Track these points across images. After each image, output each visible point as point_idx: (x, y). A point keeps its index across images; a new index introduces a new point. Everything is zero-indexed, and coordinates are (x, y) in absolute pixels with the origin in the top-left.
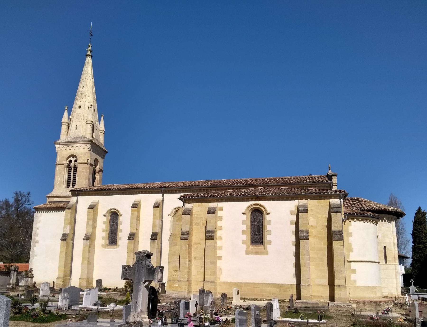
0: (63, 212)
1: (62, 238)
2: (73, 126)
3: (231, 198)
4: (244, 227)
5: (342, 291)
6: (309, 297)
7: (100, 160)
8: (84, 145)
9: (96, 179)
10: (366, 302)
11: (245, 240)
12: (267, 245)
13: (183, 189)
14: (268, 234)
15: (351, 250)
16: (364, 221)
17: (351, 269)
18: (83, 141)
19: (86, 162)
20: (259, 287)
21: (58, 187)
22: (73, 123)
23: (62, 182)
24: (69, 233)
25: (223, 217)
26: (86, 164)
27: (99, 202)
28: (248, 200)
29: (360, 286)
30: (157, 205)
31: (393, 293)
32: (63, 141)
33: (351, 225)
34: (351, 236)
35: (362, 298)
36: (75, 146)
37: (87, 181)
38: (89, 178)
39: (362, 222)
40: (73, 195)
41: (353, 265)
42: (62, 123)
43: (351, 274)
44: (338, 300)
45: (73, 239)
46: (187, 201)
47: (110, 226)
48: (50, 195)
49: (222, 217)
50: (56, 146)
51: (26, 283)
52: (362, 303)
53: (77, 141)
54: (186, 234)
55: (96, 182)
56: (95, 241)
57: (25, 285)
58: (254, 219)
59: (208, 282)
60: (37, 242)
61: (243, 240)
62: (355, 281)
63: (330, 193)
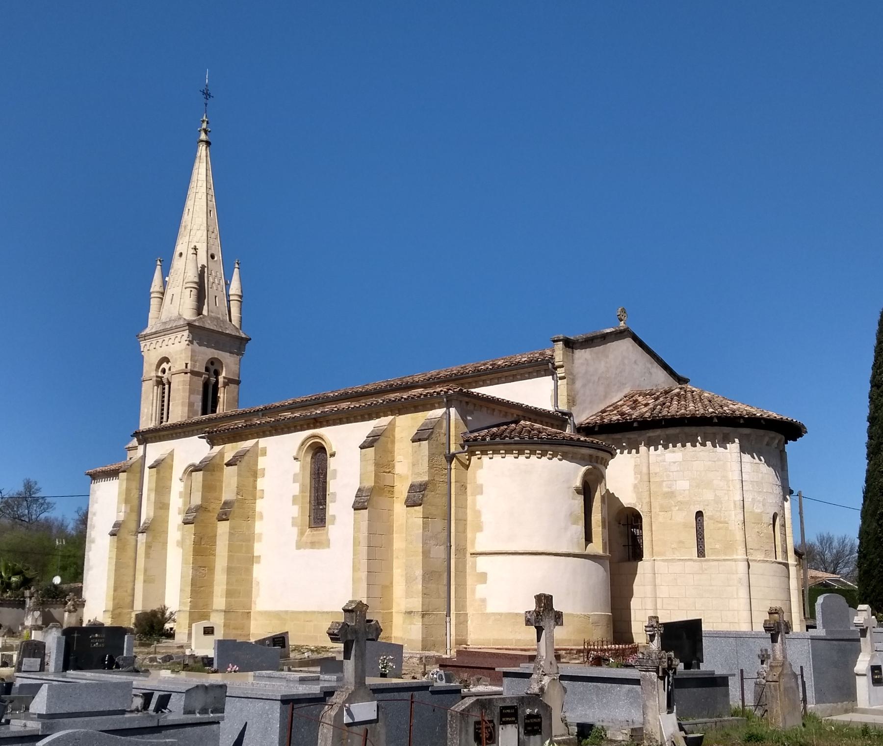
2: (168, 297)
4: (296, 489)
5: (415, 624)
8: (179, 335)
9: (219, 400)
14: (332, 502)
15: (479, 528)
16: (491, 456)
17: (477, 572)
19: (184, 370)
22: (169, 291)
23: (150, 415)
24: (123, 521)
29: (494, 614)
30: (370, 442)
32: (148, 332)
33: (481, 467)
34: (481, 493)
36: (166, 338)
37: (187, 408)
38: (189, 402)
39: (510, 458)
42: (151, 293)
46: (215, 440)
49: (264, 469)
50: (141, 342)
51: (36, 621)
53: (167, 329)
55: (219, 408)
56: (167, 533)
57: (34, 625)
58: (319, 470)
59: (217, 611)
61: (293, 518)
62: (484, 601)
63: (430, 395)
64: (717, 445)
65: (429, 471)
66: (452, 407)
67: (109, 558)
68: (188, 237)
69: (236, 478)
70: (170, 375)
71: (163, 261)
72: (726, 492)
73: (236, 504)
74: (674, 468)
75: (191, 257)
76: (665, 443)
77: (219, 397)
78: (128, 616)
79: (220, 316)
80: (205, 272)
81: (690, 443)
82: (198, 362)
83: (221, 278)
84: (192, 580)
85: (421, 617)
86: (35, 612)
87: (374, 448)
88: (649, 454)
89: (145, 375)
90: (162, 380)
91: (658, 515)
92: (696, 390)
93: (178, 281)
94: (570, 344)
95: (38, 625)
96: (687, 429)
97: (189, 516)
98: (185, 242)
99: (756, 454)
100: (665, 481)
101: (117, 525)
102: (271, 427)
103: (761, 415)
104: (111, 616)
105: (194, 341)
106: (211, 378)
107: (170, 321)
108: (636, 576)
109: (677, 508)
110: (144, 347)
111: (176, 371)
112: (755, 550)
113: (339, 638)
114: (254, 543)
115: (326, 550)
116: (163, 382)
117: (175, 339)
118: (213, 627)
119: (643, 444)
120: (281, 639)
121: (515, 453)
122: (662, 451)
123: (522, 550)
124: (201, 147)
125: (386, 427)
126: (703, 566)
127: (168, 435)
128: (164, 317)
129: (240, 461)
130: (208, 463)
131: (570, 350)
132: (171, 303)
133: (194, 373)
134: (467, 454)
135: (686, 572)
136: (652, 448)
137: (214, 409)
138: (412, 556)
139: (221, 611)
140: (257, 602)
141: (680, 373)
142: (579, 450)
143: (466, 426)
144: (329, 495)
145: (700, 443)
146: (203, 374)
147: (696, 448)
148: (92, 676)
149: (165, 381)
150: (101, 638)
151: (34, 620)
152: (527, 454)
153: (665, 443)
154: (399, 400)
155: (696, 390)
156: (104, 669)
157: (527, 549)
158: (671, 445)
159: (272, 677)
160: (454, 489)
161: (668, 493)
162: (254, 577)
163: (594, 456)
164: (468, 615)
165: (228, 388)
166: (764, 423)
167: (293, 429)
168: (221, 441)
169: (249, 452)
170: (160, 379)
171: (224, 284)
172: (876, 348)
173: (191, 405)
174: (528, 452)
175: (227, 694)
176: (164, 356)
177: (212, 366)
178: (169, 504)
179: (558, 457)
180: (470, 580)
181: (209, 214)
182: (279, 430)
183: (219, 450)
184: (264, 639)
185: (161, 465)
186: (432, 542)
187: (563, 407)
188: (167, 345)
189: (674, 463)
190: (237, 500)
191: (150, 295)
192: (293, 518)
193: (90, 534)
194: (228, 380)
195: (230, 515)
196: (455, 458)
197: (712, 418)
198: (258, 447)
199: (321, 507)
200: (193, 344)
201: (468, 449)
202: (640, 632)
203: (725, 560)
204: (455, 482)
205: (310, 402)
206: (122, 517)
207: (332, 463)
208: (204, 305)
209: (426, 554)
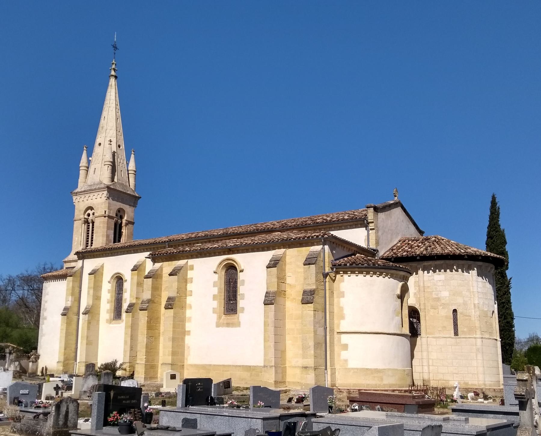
0: (65, 280)
1: (63, 313)
2: (91, 170)
3: (201, 252)
4: (215, 291)
5: (310, 375)
6: (271, 382)
7: (126, 208)
8: (101, 193)
9: (122, 234)
10: (352, 391)
11: (216, 308)
12: (239, 313)
13: (190, 242)
14: (241, 299)
15: (342, 317)
16: (349, 275)
17: (342, 343)
18: (99, 189)
19: (103, 215)
20: (228, 371)
21: (75, 248)
22: (92, 166)
23: (80, 242)
24: (70, 306)
25: (193, 278)
26: (103, 217)
27: (105, 265)
28: (220, 254)
29: (353, 369)
31: (469, 381)
32: (79, 191)
33: (343, 281)
34: (343, 297)
35: (354, 385)
36: (91, 195)
37: (105, 238)
39: (361, 276)
40: (79, 258)
41: (345, 338)
42: (80, 167)
43: (341, 351)
44: (304, 387)
45: (77, 313)
46: (156, 259)
47: (116, 296)
48: (66, 260)
49: (192, 278)
52: (346, 391)
53: (93, 189)
54: (146, 303)
56: (99, 315)
57: (15, 371)
58: (230, 280)
60: (45, 319)
61: (213, 308)
62: (346, 361)
63: (311, 238)
64: (464, 271)
65: (316, 283)
66: (326, 245)
67: (61, 329)
68: (104, 134)
69: (177, 283)
70: (94, 218)
71: (87, 147)
72: (470, 298)
73: (177, 299)
74: (440, 284)
75: (107, 146)
76: (434, 269)
77: (122, 232)
78: (72, 365)
79: (124, 183)
80: (115, 156)
81: (449, 270)
82: (112, 210)
83: (124, 160)
84: (146, 344)
85: (314, 370)
86: (16, 362)
87: (276, 268)
88: (423, 275)
89: (76, 217)
90: (88, 220)
91: (430, 311)
92: (445, 239)
93: (99, 160)
94: (376, 210)
95: (17, 371)
96: (448, 262)
97: (144, 306)
98: (102, 137)
99: (484, 277)
100: (434, 291)
101: (66, 309)
102: (198, 253)
103: (490, 255)
104: (62, 365)
105: (110, 198)
106: (119, 221)
107: (94, 184)
108: (415, 346)
109: (442, 307)
110: (75, 200)
111: (98, 215)
112: (485, 332)
113: (525, 398)
114: (186, 323)
115: (238, 329)
116: (88, 221)
117: (97, 196)
118: (175, 375)
119: (421, 269)
120: (228, 383)
121: (364, 274)
122: (432, 274)
123: (369, 331)
124: (111, 80)
125: (281, 255)
126: (457, 341)
127: (100, 254)
128: (90, 181)
129: (179, 273)
130: (155, 274)
131: (376, 213)
132: (94, 174)
133: (110, 217)
134: (334, 273)
135: (447, 344)
136: (426, 272)
137: (119, 239)
138: (307, 333)
139: (169, 364)
140: (188, 359)
141: (421, 229)
142: (399, 273)
143: (333, 257)
144: (239, 295)
145: (455, 270)
146: (114, 217)
147: (452, 272)
148: (212, 410)
149: (90, 221)
150: (202, 385)
151: (15, 368)
152: (371, 274)
153: (434, 269)
154: (290, 240)
155: (445, 239)
156: (208, 405)
157: (372, 331)
158: (437, 270)
159: (403, 417)
160: (328, 294)
161: (436, 298)
162: (186, 343)
163: (405, 276)
164: (336, 369)
165: (128, 227)
166: (491, 259)
167: (213, 254)
168: (161, 260)
169: (183, 268)
170: (86, 220)
171: (126, 164)
172: (490, 216)
173: (108, 236)
174: (372, 273)
175: (443, 431)
176: (89, 206)
177: (119, 213)
178: (101, 297)
179: (388, 277)
180: (336, 348)
181: (117, 120)
182: (203, 255)
183: (160, 266)
184: (220, 383)
185: (97, 273)
186: (318, 325)
187: (372, 246)
188: (92, 199)
189: (440, 281)
190: (177, 297)
191: (80, 169)
192: (213, 308)
193: (43, 314)
194: (128, 222)
195: (174, 306)
196: (328, 276)
197: (464, 255)
198: (188, 265)
199: (232, 302)
200: (109, 199)
201: (335, 271)
202: (418, 379)
203: (469, 338)
204: (329, 290)
205: (202, 238)
206: (69, 304)
207: (241, 276)
208: (115, 175)
209: (315, 332)
